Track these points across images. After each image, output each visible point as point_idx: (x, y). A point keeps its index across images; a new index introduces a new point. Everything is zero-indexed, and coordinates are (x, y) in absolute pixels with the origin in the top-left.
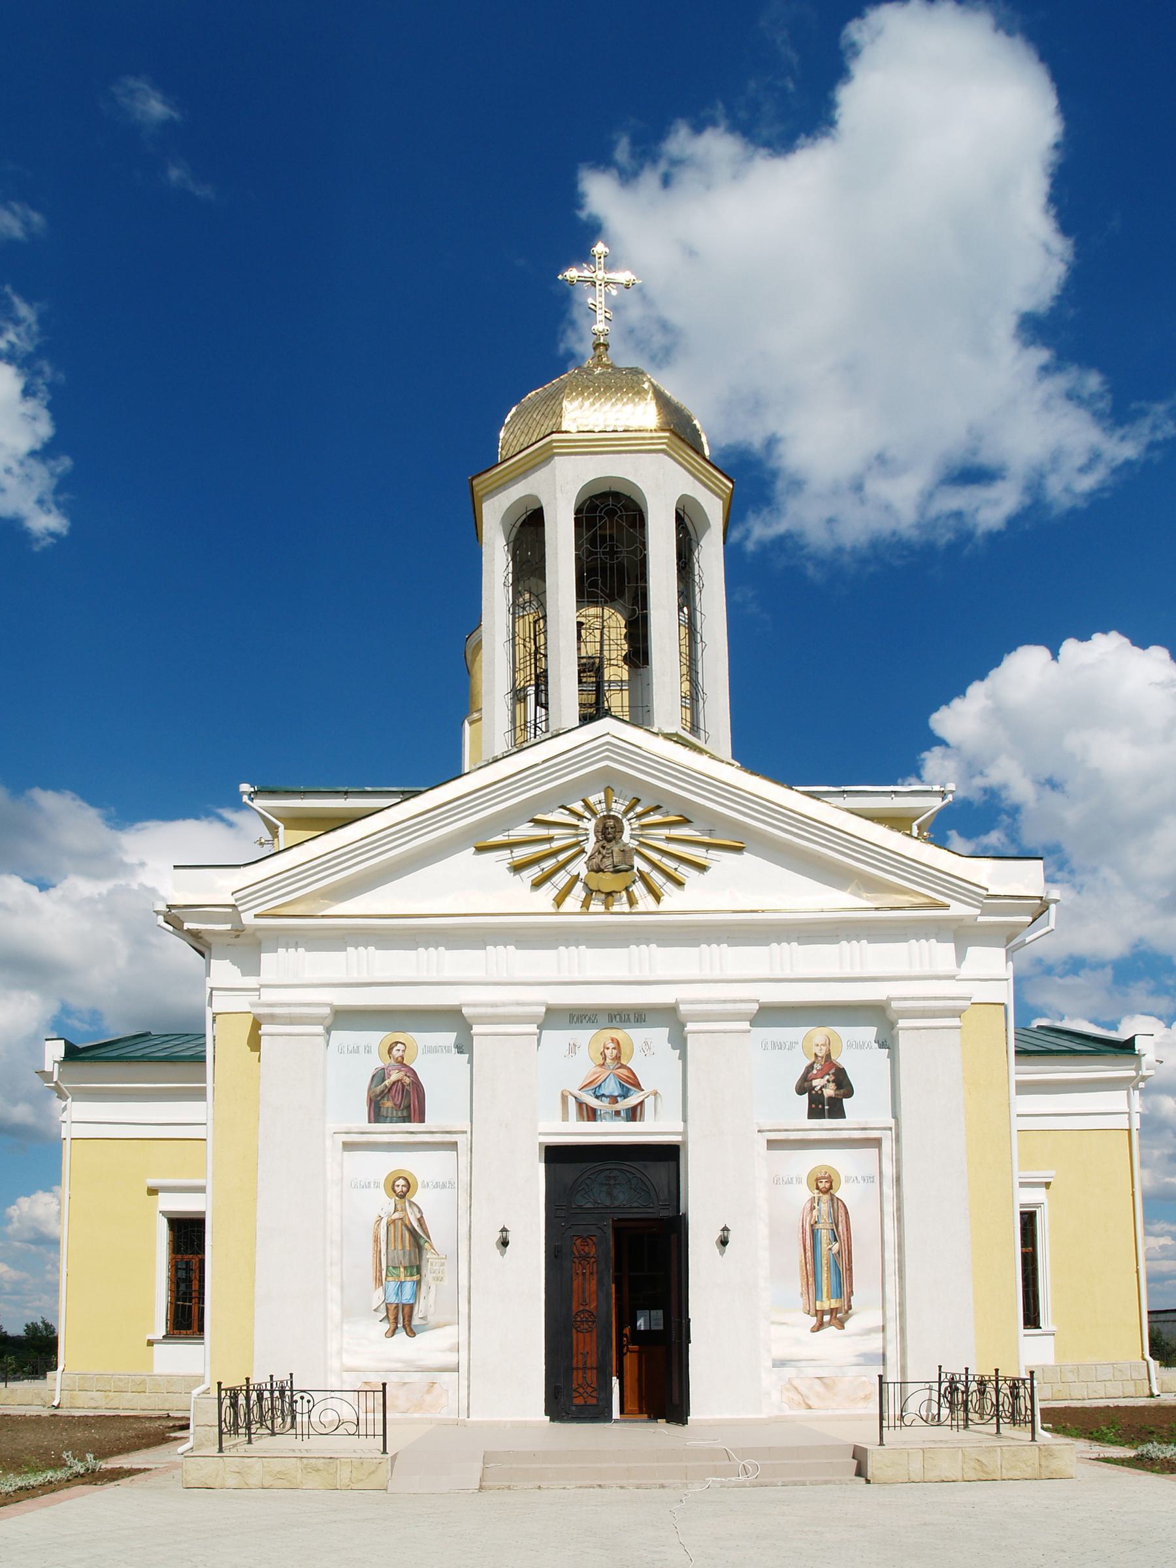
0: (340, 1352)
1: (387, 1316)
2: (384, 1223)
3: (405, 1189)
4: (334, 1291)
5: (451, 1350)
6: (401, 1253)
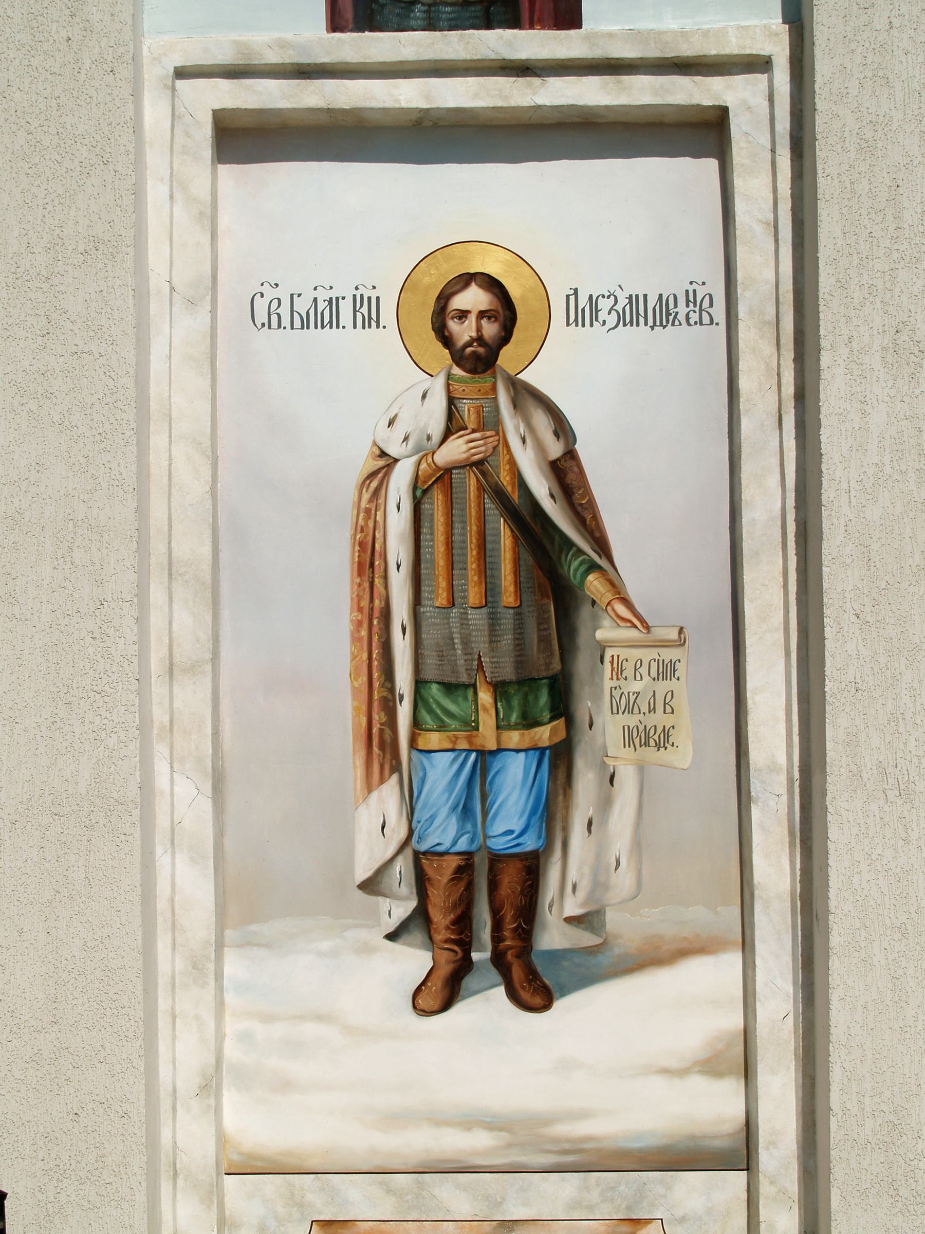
0: (211, 1086)
1: (421, 917)
2: (400, 482)
3: (490, 329)
4: (184, 797)
5: (710, 1066)
6: (479, 619)
